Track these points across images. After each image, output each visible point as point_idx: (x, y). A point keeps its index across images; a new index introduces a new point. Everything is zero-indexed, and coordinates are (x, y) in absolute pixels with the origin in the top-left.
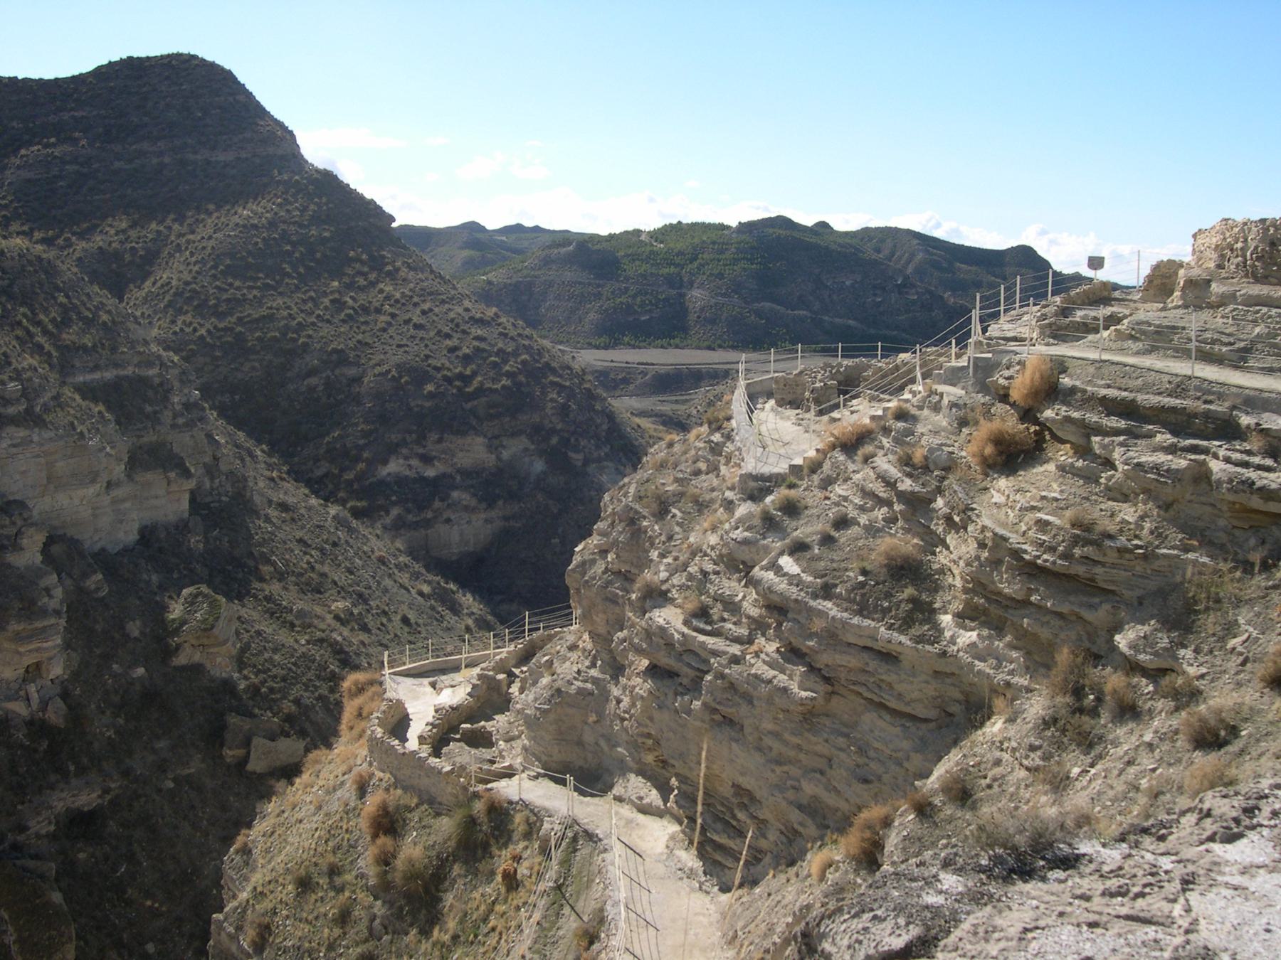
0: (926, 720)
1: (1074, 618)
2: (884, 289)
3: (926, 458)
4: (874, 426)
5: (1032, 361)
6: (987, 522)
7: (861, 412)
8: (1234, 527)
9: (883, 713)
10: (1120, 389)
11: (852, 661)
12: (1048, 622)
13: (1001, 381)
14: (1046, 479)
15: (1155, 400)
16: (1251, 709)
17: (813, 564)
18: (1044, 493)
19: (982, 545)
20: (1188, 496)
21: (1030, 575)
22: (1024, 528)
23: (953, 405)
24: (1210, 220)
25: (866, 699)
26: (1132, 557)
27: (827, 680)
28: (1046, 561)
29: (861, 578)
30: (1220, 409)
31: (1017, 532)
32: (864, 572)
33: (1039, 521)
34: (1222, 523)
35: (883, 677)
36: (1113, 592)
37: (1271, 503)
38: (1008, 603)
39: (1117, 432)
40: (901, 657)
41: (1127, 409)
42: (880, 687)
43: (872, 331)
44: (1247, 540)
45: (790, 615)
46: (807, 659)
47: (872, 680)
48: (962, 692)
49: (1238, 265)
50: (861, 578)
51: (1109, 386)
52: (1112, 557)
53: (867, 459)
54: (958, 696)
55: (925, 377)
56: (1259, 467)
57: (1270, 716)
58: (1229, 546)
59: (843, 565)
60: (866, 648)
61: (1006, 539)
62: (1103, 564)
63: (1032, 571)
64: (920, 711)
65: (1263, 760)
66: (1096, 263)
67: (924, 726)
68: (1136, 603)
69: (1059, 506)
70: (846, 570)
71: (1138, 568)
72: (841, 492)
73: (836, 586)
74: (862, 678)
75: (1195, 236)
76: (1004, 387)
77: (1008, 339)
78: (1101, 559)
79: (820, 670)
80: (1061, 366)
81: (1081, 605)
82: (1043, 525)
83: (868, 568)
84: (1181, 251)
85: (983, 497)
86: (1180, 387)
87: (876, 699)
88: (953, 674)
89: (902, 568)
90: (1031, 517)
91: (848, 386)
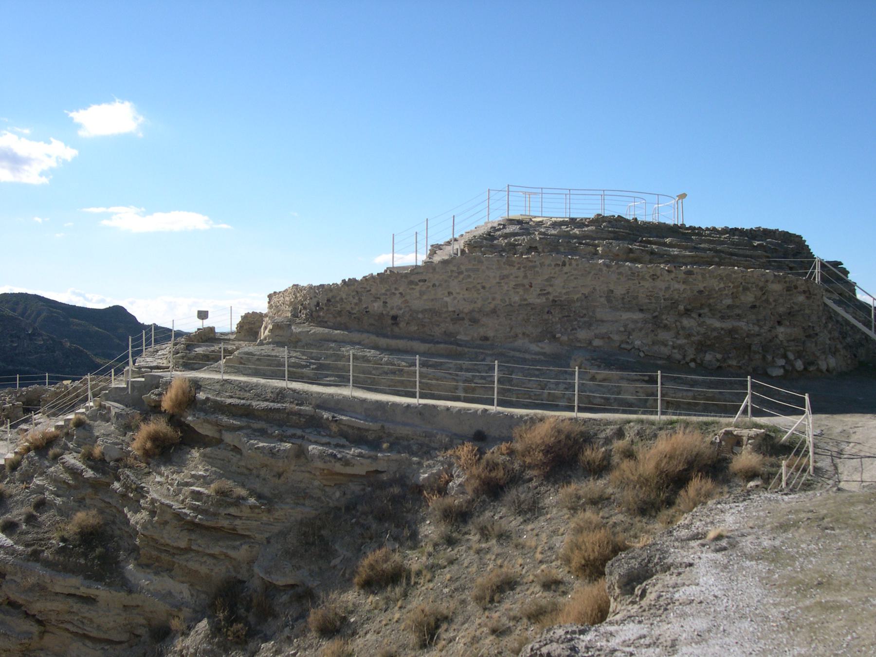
0: (120, 643)
1: (223, 557)
2: (19, 337)
3: (103, 454)
4: (58, 432)
5: (175, 384)
6: (155, 496)
7: (44, 424)
8: (325, 485)
9: (87, 642)
10: (239, 398)
11: (58, 605)
12: (205, 562)
13: (153, 397)
14: (196, 463)
15: (264, 404)
16: (354, 604)
17: (23, 537)
18: (193, 473)
19: (153, 513)
20: (292, 468)
21: (189, 530)
22: (182, 498)
23: (118, 416)
24: (283, 284)
25: (72, 633)
26: (260, 511)
27: (40, 622)
28: (200, 519)
29: (61, 544)
30: (307, 408)
31: (177, 501)
32: (63, 539)
33: (193, 492)
34: (316, 483)
35: (87, 615)
36: (248, 536)
37: (347, 468)
38: (175, 551)
39: (239, 428)
40: (98, 599)
41: (246, 412)
42: (83, 623)
43: (10, 367)
44: (334, 493)
45: (7, 577)
46: (23, 609)
47: (76, 618)
48: (145, 619)
49: (306, 314)
50: (61, 544)
51: (231, 397)
52: (246, 512)
53: (56, 458)
54: (144, 622)
55: (95, 395)
56: (337, 446)
57: (367, 607)
58: (323, 498)
59: (46, 536)
60: (70, 595)
61: (171, 507)
62: (240, 518)
63: (193, 527)
64: (115, 637)
65: (368, 636)
66: (203, 315)
67: (118, 647)
68: (265, 542)
69: (205, 481)
70: (50, 539)
71: (264, 518)
72: (38, 482)
73: (43, 551)
74: (67, 617)
75: (270, 296)
76: (155, 401)
77: (152, 368)
78: (239, 514)
79: (34, 616)
80: (197, 385)
81: (228, 547)
82: (197, 495)
83: (66, 536)
84: (262, 307)
85: (149, 478)
86: (280, 395)
87: (80, 632)
88: (138, 606)
89: (92, 533)
90: (186, 490)
91: (31, 406)
